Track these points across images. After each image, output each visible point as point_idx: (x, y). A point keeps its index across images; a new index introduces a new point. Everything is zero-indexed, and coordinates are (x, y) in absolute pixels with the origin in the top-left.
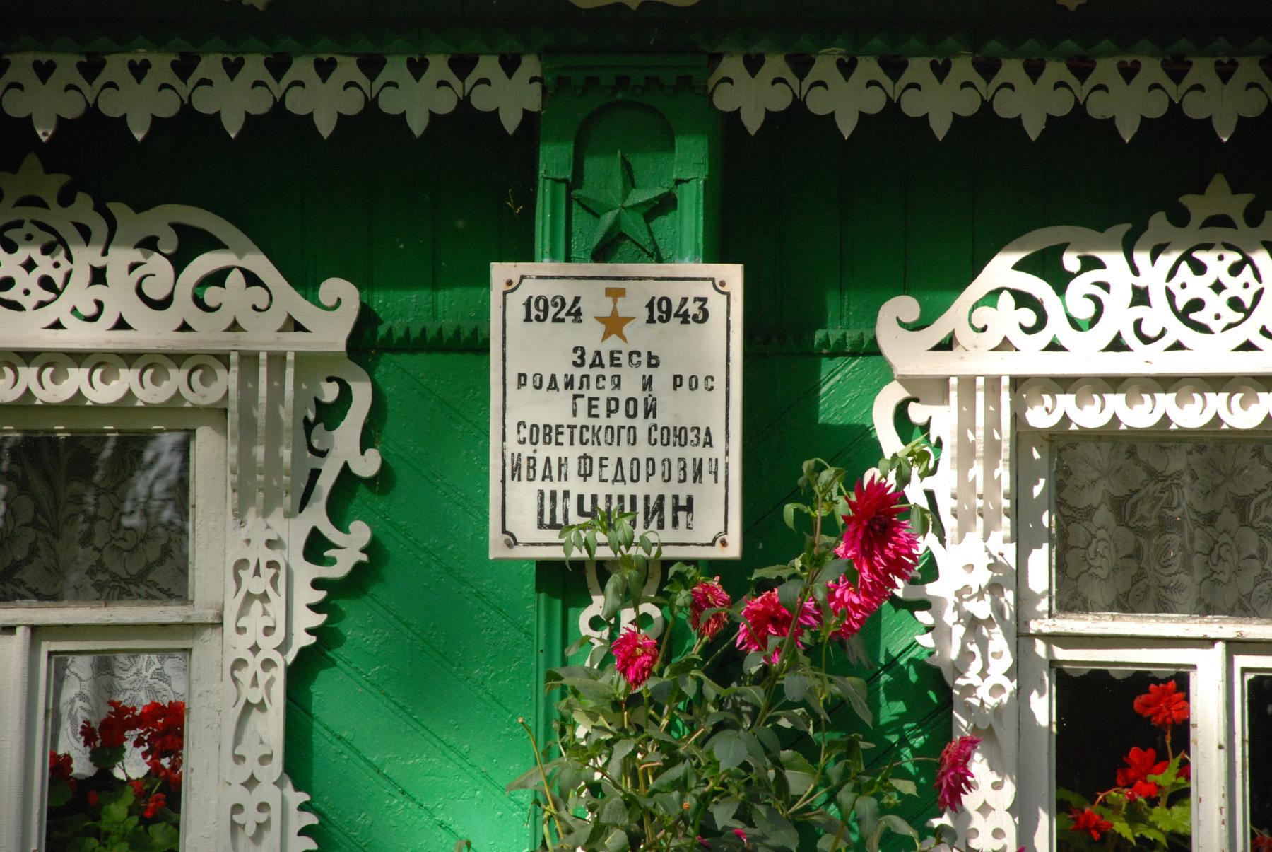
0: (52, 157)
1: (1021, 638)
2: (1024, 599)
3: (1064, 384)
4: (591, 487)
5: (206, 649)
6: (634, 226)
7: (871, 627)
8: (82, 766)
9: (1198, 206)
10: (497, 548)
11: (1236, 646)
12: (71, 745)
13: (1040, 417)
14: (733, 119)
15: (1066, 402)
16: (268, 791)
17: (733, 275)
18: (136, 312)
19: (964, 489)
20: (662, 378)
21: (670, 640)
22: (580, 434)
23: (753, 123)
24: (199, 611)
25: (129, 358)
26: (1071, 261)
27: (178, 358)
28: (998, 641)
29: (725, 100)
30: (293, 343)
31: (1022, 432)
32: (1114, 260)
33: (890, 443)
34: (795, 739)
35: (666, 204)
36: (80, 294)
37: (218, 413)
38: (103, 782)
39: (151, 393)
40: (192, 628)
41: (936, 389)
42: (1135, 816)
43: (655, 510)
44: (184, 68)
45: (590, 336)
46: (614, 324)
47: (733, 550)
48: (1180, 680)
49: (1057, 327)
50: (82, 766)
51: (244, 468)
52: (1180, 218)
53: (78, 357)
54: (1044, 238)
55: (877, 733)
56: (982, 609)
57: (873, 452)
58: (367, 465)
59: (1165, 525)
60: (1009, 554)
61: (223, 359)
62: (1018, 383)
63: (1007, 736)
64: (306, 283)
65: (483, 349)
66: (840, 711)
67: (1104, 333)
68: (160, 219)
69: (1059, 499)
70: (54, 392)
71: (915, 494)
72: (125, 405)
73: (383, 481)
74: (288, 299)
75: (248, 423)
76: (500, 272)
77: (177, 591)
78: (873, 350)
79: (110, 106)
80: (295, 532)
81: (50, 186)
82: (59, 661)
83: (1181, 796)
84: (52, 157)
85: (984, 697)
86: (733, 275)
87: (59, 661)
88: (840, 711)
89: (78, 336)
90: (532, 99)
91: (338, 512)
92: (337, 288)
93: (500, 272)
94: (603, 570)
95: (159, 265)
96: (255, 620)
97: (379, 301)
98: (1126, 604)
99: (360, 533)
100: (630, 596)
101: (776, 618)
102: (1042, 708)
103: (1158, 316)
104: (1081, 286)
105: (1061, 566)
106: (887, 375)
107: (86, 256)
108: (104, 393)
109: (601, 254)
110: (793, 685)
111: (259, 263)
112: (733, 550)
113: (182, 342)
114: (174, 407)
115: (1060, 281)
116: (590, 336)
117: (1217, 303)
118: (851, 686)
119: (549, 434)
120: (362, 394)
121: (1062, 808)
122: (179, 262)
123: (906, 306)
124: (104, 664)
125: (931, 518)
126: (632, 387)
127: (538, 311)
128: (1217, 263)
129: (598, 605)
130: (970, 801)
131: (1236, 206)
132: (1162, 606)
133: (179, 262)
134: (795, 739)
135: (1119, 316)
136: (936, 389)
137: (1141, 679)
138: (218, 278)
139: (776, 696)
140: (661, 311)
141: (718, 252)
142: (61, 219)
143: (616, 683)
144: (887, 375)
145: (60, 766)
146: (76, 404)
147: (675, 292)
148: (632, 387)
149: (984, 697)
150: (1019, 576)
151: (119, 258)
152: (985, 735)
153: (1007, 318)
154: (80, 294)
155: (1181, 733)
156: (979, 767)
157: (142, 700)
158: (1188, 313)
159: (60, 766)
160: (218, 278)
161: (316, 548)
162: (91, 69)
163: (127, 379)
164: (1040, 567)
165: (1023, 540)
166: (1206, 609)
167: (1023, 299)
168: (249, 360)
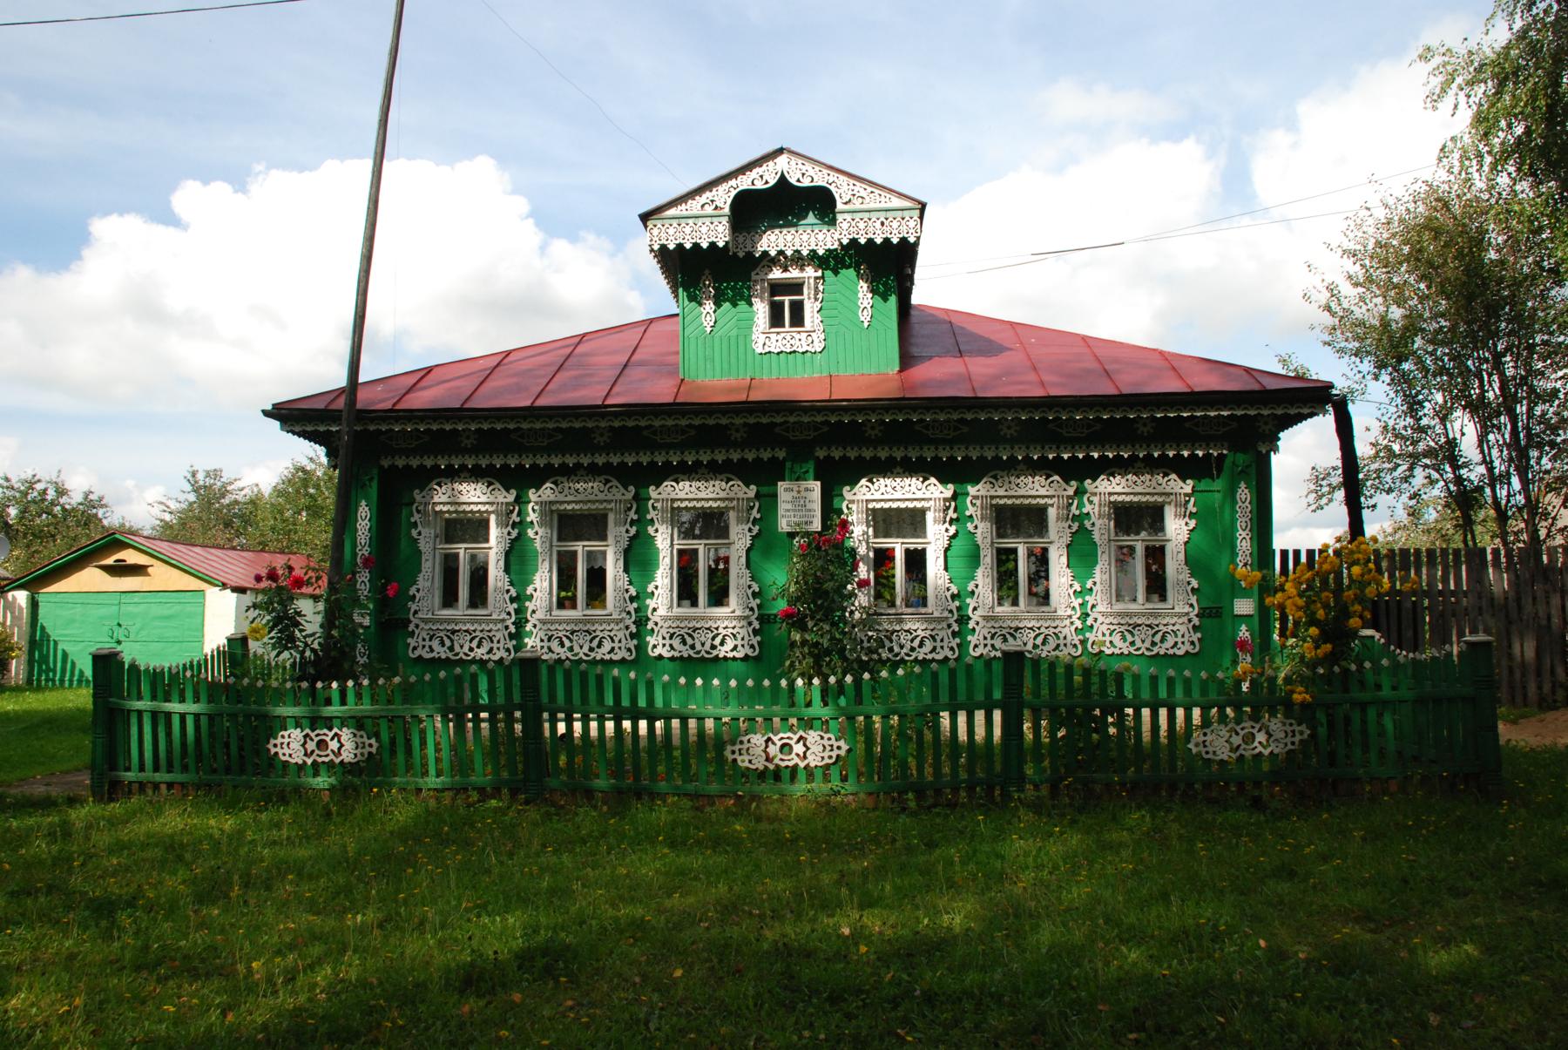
0: (585, 469)
1: (868, 543)
2: (868, 537)
3: (998, 497)
4: (795, 519)
5: (732, 547)
6: (802, 476)
7: (843, 542)
8: (713, 566)
9: (895, 471)
10: (780, 530)
11: (903, 543)
12: (711, 563)
13: (870, 506)
14: (818, 457)
15: (874, 503)
16: (743, 570)
17: (819, 483)
18: (720, 492)
19: (858, 519)
20: (807, 501)
21: (809, 544)
22: (794, 510)
23: (821, 458)
24: (731, 541)
25: (719, 499)
26: (875, 480)
27: (727, 499)
28: (864, 543)
29: (817, 454)
30: (745, 496)
31: (867, 509)
32: (882, 480)
33: (846, 511)
34: (830, 561)
35: (807, 472)
36: (711, 489)
37: (733, 508)
38: (717, 569)
39: (723, 505)
40: (730, 544)
41: (852, 502)
42: (886, 571)
43: (806, 523)
44: (727, 451)
45: (795, 494)
46: (799, 492)
47: (819, 529)
48: (893, 549)
49: (873, 491)
50: (713, 566)
51: (738, 518)
52: (892, 473)
53: (711, 499)
54: (871, 476)
55: (844, 559)
56: (861, 538)
57: (842, 513)
58: (758, 516)
59: (891, 524)
60: (866, 529)
61: (1054, 496)
62: (867, 501)
63: (865, 559)
64: (748, 486)
65: (776, 496)
66: (838, 556)
67: (880, 492)
68: (723, 476)
69: (874, 519)
70: (707, 505)
71: (850, 519)
72: (718, 507)
73: (761, 518)
74: (745, 489)
75: (738, 510)
76: (779, 483)
77: (728, 538)
78: (842, 495)
79: (715, 458)
80: (746, 528)
81: (1142, 465)
82: (709, 549)
83: (894, 568)
84: (706, 466)
85: (861, 553)
86: (819, 483)
87: (709, 549)
88: (838, 556)
89: (711, 496)
90: (784, 454)
91: (754, 524)
92: (752, 487)
93: (779, 483)
94: (798, 533)
95: (724, 483)
96: (740, 542)
97: (760, 489)
98: (885, 537)
99: (757, 527)
100: (803, 537)
101: (828, 541)
102: (871, 554)
103: (889, 489)
104: (1000, 481)
105: (875, 531)
106: (845, 499)
107: (712, 483)
108: (715, 505)
109: (797, 480)
110: (830, 552)
111: (740, 483)
112: (819, 529)
113: (606, 498)
114: (726, 507)
115: (873, 483)
116: (795, 494)
117: (1022, 484)
118: (839, 551)
119: (788, 510)
120: (517, 508)
121: (875, 571)
122: (727, 483)
123: (848, 488)
124: (716, 550)
125: (852, 524)
126: (802, 502)
127: (786, 490)
128: (898, 480)
129: (797, 539)
130: (859, 570)
131: (901, 471)
132: (891, 537)
133: (727, 483)
134: (830, 561)
135: (883, 489)
136: (852, 502)
137: (888, 549)
138: (733, 486)
139: (827, 554)
140: (807, 490)
141: (816, 479)
142: (586, 478)
143: (800, 552)
144: (845, 499)
145: (710, 566)
146: (710, 507)
147: (809, 486)
148: (802, 502)
149: (861, 553)
150: (867, 533)
151: (717, 483)
152: (862, 559)
153: (865, 490)
154: (711, 489)
155: (894, 557)
156: (861, 564)
157: (722, 555)
158: (894, 488)
159: (710, 566)
160: (611, 487)
161: (750, 530)
162: (697, 453)
163: (719, 502)
164: (871, 531)
165: (868, 526)
166: (898, 537)
167: (991, 483)
168: (738, 499)
